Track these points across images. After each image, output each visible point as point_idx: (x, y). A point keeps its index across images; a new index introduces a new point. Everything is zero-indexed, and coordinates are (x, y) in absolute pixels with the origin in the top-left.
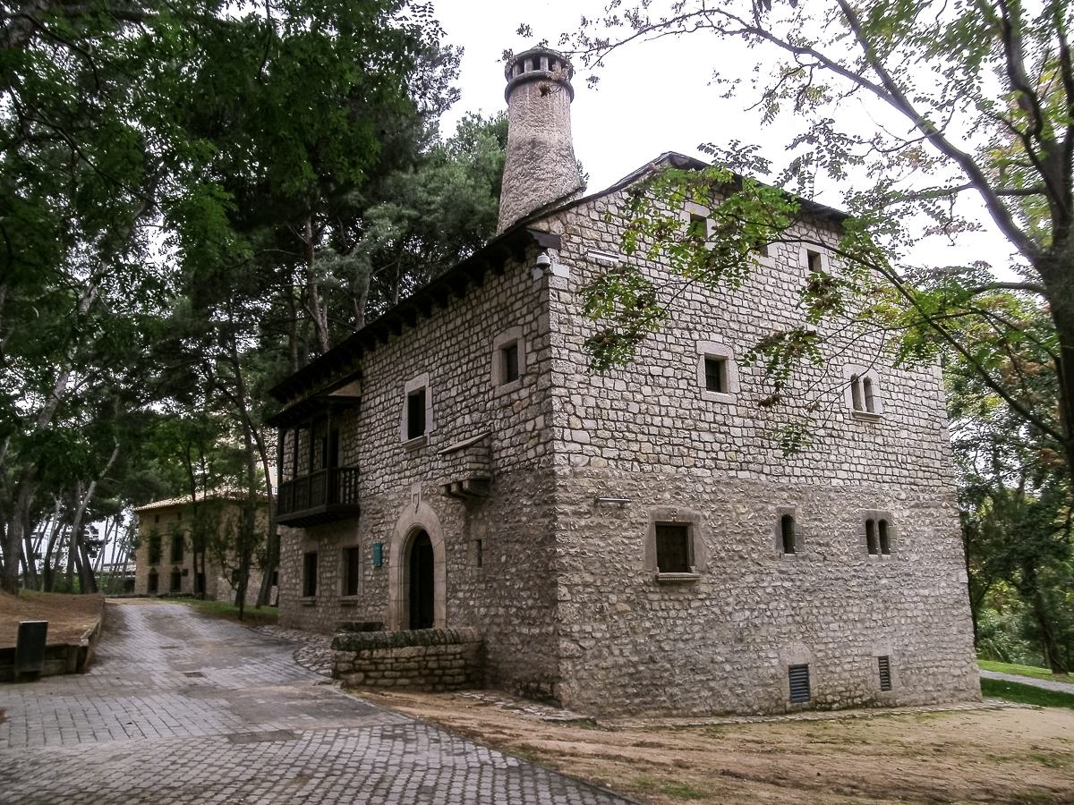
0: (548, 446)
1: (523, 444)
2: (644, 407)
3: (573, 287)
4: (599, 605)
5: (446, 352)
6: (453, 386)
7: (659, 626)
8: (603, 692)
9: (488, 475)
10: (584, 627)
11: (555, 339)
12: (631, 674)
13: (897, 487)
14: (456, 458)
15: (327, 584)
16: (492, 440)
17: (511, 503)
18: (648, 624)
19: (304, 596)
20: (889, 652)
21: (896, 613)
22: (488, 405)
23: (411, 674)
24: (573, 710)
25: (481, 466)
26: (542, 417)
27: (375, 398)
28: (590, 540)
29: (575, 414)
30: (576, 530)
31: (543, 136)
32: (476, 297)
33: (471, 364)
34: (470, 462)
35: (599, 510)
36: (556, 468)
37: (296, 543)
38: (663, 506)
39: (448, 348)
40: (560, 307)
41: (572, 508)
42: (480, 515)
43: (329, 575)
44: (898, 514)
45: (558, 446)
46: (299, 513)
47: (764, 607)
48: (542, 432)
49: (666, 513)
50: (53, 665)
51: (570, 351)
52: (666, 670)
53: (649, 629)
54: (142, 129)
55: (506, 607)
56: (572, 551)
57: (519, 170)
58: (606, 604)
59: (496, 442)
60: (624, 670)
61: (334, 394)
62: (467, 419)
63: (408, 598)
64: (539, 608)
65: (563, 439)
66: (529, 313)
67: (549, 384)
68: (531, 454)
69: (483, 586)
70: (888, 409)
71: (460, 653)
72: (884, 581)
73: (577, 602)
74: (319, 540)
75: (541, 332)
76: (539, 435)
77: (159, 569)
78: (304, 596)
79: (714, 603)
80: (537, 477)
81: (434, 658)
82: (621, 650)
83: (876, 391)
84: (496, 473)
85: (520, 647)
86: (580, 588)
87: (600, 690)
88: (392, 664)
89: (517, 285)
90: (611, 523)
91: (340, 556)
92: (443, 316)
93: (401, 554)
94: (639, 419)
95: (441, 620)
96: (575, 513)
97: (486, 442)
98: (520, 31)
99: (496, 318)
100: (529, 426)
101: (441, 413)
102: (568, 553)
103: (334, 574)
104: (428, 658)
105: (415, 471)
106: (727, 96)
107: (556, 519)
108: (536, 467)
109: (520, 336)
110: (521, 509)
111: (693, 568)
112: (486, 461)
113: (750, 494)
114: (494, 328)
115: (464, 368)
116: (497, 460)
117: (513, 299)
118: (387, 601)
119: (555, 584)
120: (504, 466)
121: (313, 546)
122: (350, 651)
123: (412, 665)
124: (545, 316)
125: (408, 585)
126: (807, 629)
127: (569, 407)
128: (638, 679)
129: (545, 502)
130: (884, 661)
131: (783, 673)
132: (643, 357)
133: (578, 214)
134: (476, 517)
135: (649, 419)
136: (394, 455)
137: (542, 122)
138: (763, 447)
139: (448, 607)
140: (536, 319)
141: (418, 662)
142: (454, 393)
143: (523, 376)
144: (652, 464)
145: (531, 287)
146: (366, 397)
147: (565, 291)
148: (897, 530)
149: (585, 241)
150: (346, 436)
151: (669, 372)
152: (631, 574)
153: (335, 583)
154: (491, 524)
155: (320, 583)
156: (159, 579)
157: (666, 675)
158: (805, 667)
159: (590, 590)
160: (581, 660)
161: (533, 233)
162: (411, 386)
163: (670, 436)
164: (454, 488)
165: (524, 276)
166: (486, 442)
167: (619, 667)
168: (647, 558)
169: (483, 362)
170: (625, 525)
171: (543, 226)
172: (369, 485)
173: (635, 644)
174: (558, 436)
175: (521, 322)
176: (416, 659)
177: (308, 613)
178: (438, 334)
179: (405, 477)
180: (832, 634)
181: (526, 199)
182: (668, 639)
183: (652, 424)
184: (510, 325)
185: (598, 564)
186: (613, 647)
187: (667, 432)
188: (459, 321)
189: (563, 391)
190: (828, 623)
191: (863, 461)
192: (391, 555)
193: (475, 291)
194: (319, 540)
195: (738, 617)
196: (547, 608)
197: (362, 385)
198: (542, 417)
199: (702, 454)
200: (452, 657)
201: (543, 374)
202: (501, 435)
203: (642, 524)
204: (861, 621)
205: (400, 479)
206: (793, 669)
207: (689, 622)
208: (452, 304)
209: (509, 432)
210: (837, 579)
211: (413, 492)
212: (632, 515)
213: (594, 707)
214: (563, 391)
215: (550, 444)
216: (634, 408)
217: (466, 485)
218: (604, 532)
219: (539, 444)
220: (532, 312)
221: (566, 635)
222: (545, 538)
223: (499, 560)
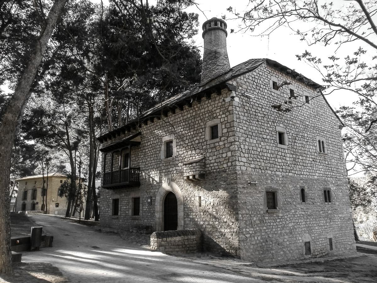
0: (233, 163)
3: (240, 105)
7: (268, 229)
9: (204, 173)
11: (236, 124)
12: (260, 246)
13: (332, 179)
15: (124, 211)
16: (206, 160)
18: (265, 228)
19: (112, 215)
20: (332, 237)
21: (333, 223)
29: (242, 151)
31: (219, 50)
34: (199, 168)
36: (237, 171)
37: (108, 195)
39: (184, 125)
40: (237, 112)
43: (125, 207)
44: (333, 188)
45: (237, 163)
46: (114, 185)
47: (297, 221)
50: (42, 244)
52: (270, 245)
53: (265, 230)
57: (210, 62)
61: (132, 140)
63: (163, 217)
66: (223, 114)
70: (329, 152)
71: (195, 239)
72: (329, 212)
77: (26, 202)
78: (112, 215)
79: (283, 220)
81: (187, 241)
83: (325, 146)
86: (245, 215)
89: (218, 104)
90: (254, 191)
91: (131, 201)
95: (181, 226)
97: (204, 161)
98: (228, 9)
99: (207, 115)
100: (224, 155)
103: (128, 207)
104: (185, 241)
106: (302, 40)
107: (237, 190)
109: (219, 122)
110: (221, 186)
111: (277, 208)
112: (204, 168)
113: (293, 181)
125: (163, 212)
126: (310, 230)
129: (232, 184)
130: (330, 240)
131: (303, 244)
133: (241, 79)
138: (295, 164)
139: (185, 221)
143: (221, 137)
146: (143, 142)
147: (238, 107)
148: (333, 194)
151: (268, 137)
153: (128, 211)
155: (121, 210)
156: (26, 206)
157: (270, 246)
158: (309, 242)
164: (191, 177)
165: (221, 101)
166: (204, 161)
173: (262, 236)
174: (237, 159)
176: (181, 241)
177: (114, 221)
178: (179, 120)
180: (316, 231)
181: (214, 72)
184: (214, 118)
188: (189, 116)
190: (315, 227)
191: (323, 170)
195: (290, 225)
197: (141, 137)
199: (278, 167)
200: (192, 240)
202: (211, 158)
203: (262, 192)
204: (324, 226)
206: (306, 243)
207: (277, 227)
210: (317, 211)
216: (259, 150)
219: (229, 162)
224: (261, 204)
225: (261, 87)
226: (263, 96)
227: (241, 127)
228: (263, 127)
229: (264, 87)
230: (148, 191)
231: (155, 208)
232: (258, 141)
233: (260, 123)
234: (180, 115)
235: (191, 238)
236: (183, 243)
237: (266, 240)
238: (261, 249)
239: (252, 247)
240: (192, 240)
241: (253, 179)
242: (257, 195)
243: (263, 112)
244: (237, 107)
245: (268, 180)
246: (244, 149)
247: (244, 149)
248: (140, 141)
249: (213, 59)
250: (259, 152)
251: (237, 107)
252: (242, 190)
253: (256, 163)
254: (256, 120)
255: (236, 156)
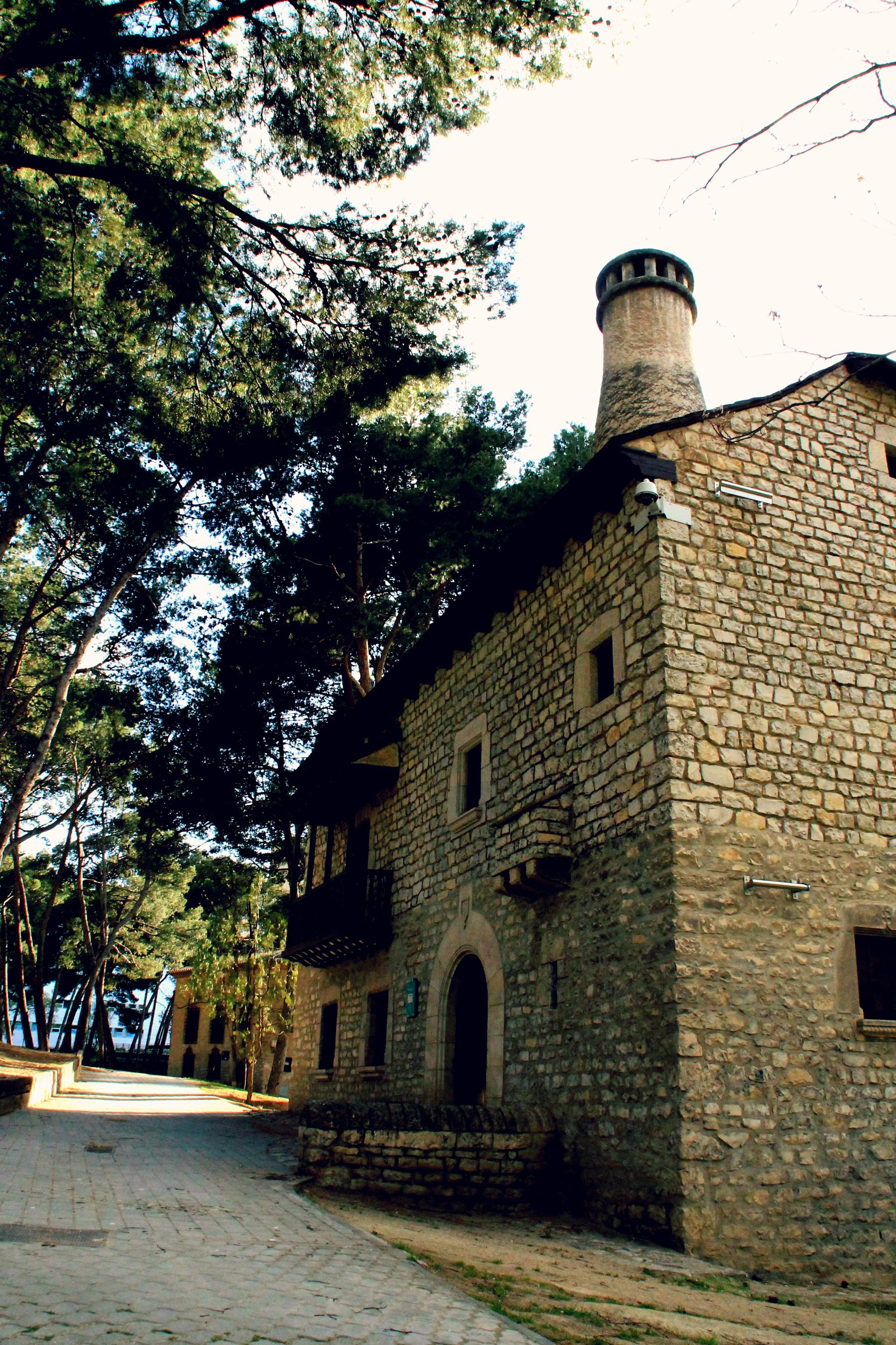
1: (620, 795)
2: (826, 734)
3: (698, 539)
4: (754, 1068)
5: (510, 677)
6: (520, 724)
7: (864, 1114)
8: (764, 1229)
9: (568, 853)
10: (727, 1108)
11: (669, 616)
12: (816, 1199)
14: (518, 828)
16: (574, 798)
17: (602, 896)
18: (845, 1109)
22: (569, 743)
23: (428, 1178)
24: (707, 1259)
25: (556, 838)
26: (651, 744)
27: (415, 766)
28: (738, 954)
29: (707, 738)
30: (711, 934)
31: (651, 358)
32: (551, 584)
33: (545, 685)
35: (754, 900)
36: (674, 826)
37: (314, 992)
38: (867, 902)
40: (677, 567)
41: (705, 895)
42: (556, 922)
45: (678, 788)
48: (652, 770)
49: (872, 914)
51: (697, 636)
52: (881, 1196)
53: (847, 1118)
54: (164, 469)
55: (593, 1072)
56: (705, 970)
57: (617, 406)
58: (769, 1068)
59: (581, 798)
60: (803, 1191)
62: (539, 772)
64: (648, 1072)
65: (686, 778)
67: (660, 688)
68: (634, 808)
69: (559, 1038)
73: (714, 1061)
74: (341, 984)
75: (646, 610)
76: (646, 776)
77: (196, 1048)
80: (644, 846)
81: (469, 1154)
82: (797, 1154)
84: (580, 849)
85: (614, 1141)
86: (720, 1037)
87: (757, 1223)
88: (396, 1157)
89: (611, 547)
90: (775, 925)
92: (507, 624)
93: (442, 995)
94: (819, 754)
96: (709, 904)
99: (580, 606)
101: (502, 770)
102: (696, 973)
105: (464, 865)
107: (674, 912)
108: (642, 828)
109: (617, 623)
110: (618, 903)
112: (564, 830)
114: (578, 621)
115: (535, 695)
116: (582, 827)
117: (605, 570)
118: (421, 1072)
119: (673, 1027)
120: (592, 836)
121: (333, 994)
122: (327, 1129)
123: (432, 1162)
124: (653, 582)
127: (696, 726)
128: (833, 1209)
129: (657, 885)
132: (822, 654)
134: (549, 925)
135: (835, 755)
136: (438, 846)
137: (649, 341)
139: (505, 1077)
140: (639, 591)
141: (443, 1158)
142: (519, 735)
143: (621, 685)
144: (845, 829)
145: (631, 544)
147: (684, 543)
149: (715, 472)
150: (379, 827)
151: (866, 680)
152: (812, 1018)
153: (357, 1047)
154: (572, 933)
159: (736, 1041)
160: (723, 1167)
161: (630, 455)
162: (463, 739)
163: (874, 785)
164: (514, 877)
167: (796, 1186)
168: (840, 989)
169: (562, 678)
170: (800, 931)
171: (646, 445)
172: (404, 895)
173: (823, 1145)
174: (678, 771)
175: (617, 601)
179: (452, 877)
182: (883, 1138)
183: (842, 763)
184: (601, 610)
185: (752, 997)
186: (782, 1145)
187: (867, 777)
188: (528, 626)
189: (685, 700)
192: (430, 998)
193: (550, 575)
194: (341, 984)
196: (659, 1070)
197: (401, 751)
198: (651, 744)
201: (653, 673)
203: (830, 930)
205: (445, 880)
208: (520, 603)
209: (601, 780)
211: (461, 898)
212: (811, 913)
213: (747, 1255)
214: (685, 700)
215: (664, 787)
216: (810, 734)
217: (531, 869)
218: (762, 941)
219: (645, 790)
220: (635, 582)
221: (693, 1120)
222: (657, 948)
223: (583, 993)
224: (824, 992)
225: (818, 468)
226: (832, 504)
227: (702, 631)
228: (836, 635)
229: (839, 468)
230: (410, 962)
231: (424, 1029)
232: (803, 696)
233: (819, 618)
234: (504, 631)
235: (496, 1145)
236: (451, 1162)
237: (852, 1171)
238: (819, 1215)
239: (759, 1196)
240: (499, 1156)
241: (772, 870)
242: (800, 946)
243: (833, 569)
244: (680, 547)
245: (868, 876)
246: (720, 725)
247: (720, 725)
248: (397, 765)
249: (628, 395)
250: (811, 745)
251: (680, 547)
252: (702, 915)
253: (793, 793)
254: (793, 602)
255: (670, 755)
